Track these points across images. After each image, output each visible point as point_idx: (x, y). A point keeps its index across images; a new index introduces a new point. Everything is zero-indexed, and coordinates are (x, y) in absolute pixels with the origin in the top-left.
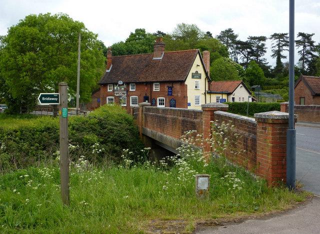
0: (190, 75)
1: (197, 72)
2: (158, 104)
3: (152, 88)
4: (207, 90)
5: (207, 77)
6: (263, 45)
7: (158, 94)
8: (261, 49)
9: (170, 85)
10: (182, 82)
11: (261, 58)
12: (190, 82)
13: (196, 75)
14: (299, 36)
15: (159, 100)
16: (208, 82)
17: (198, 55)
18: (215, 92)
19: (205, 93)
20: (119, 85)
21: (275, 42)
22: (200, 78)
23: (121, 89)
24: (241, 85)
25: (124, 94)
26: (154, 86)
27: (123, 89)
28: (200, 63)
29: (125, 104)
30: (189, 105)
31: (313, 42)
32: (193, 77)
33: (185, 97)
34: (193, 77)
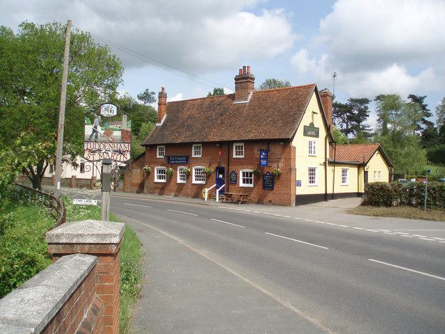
0: (300, 130)
1: (312, 124)
2: (194, 177)
3: (230, 152)
4: (328, 157)
5: (329, 135)
6: (366, 108)
7: (240, 163)
8: (363, 114)
9: (264, 148)
10: (287, 141)
11: (364, 123)
12: (300, 142)
13: (311, 131)
14: (409, 98)
15: (244, 173)
16: (330, 143)
17: (314, 93)
18: (343, 161)
19: (325, 164)
20: (105, 120)
21: (380, 103)
22: (317, 135)
23: (108, 133)
24: (377, 152)
25: (121, 152)
26: (234, 148)
27: (117, 134)
28: (317, 110)
29: (251, 183)
30: (299, 184)
31: (426, 105)
32: (305, 134)
33: (290, 170)
34: (305, 134)
